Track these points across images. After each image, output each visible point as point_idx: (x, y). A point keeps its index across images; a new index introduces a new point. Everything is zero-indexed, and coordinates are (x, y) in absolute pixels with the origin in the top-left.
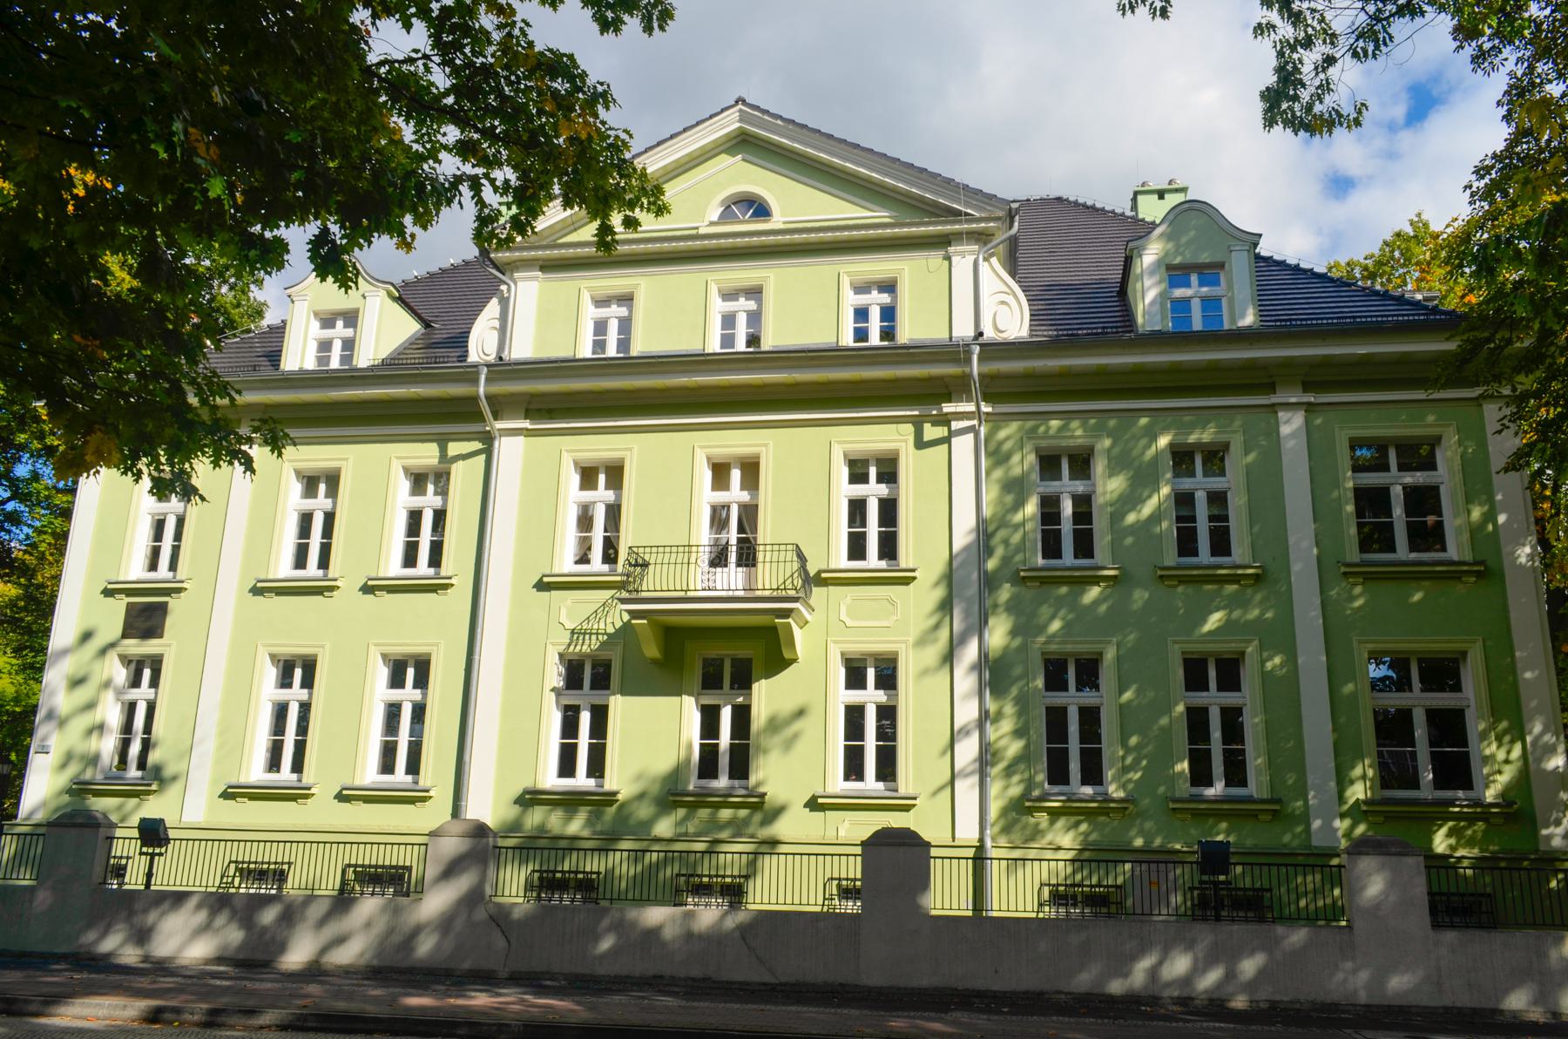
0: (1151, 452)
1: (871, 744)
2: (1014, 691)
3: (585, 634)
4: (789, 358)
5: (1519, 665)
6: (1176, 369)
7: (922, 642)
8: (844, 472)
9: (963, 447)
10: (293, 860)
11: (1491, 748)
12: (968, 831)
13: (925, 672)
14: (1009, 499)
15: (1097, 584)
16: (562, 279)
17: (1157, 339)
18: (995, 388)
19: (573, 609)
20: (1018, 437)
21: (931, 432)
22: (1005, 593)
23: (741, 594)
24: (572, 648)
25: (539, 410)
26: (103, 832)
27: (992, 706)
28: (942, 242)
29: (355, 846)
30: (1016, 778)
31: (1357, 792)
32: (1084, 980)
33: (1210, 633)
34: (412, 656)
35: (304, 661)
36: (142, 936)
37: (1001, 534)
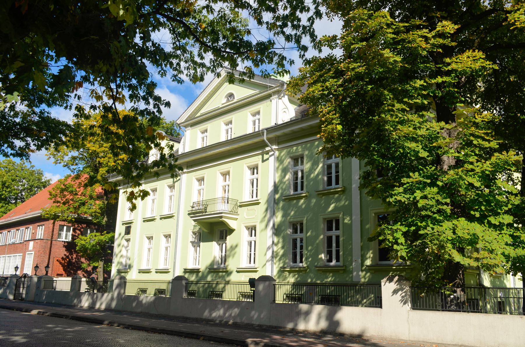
2: (282, 235)
4: (243, 138)
6: (302, 130)
7: (262, 221)
10: (340, 295)
14: (283, 174)
15: (302, 199)
16: (194, 128)
18: (272, 141)
22: (281, 204)
25: (189, 166)
26: (78, 280)
27: (276, 240)
30: (281, 261)
31: (368, 262)
32: (206, 314)
33: (331, 211)
37: (281, 185)
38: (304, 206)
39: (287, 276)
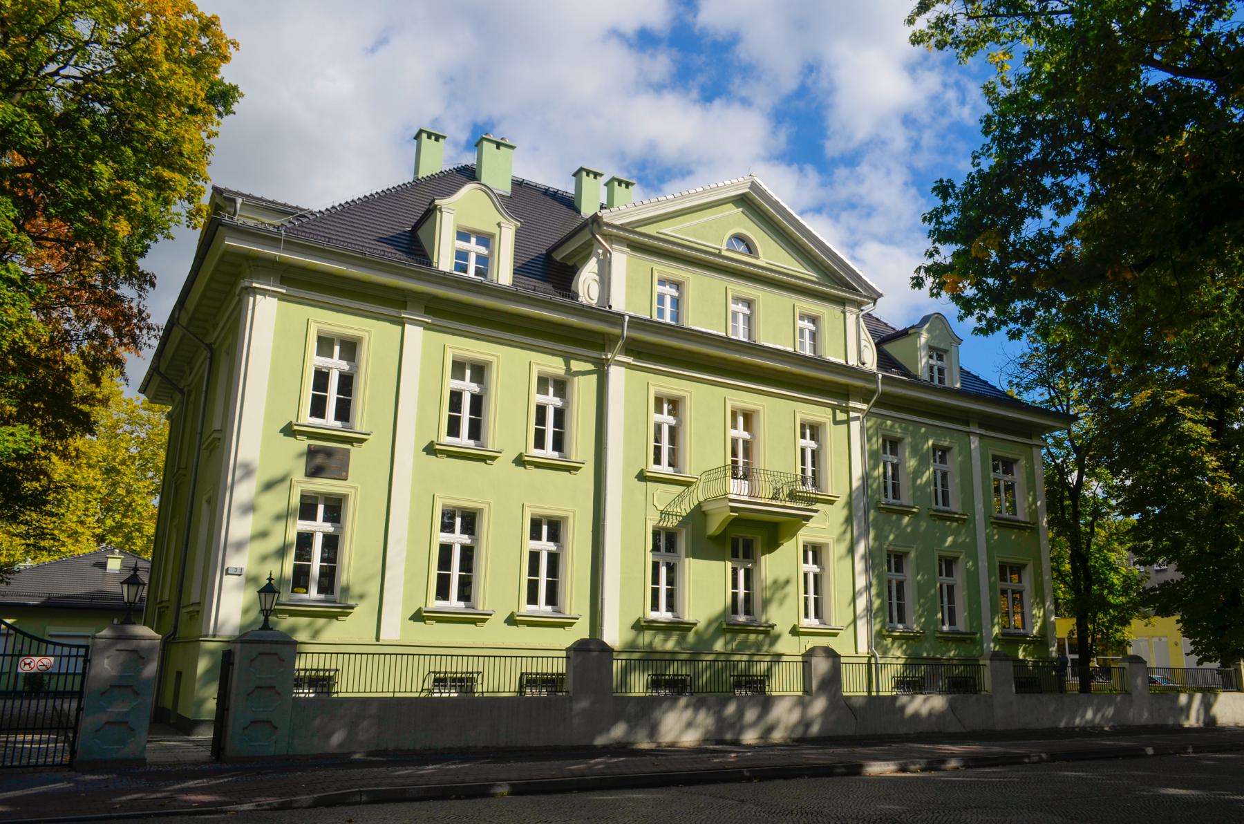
0: (926, 447)
1: (455, 573)
3: (669, 514)
5: (1044, 573)
8: (313, 345)
9: (855, 426)
11: (1035, 612)
12: (863, 648)
13: (840, 558)
17: (586, 311)
19: (663, 496)
20: (875, 427)
21: (841, 416)
23: (746, 499)
24: (661, 523)
28: (842, 302)
29: (388, 657)
33: (948, 547)
34: (546, 517)
35: (462, 512)
36: (653, 730)
38: (909, 529)
39: (890, 646)
